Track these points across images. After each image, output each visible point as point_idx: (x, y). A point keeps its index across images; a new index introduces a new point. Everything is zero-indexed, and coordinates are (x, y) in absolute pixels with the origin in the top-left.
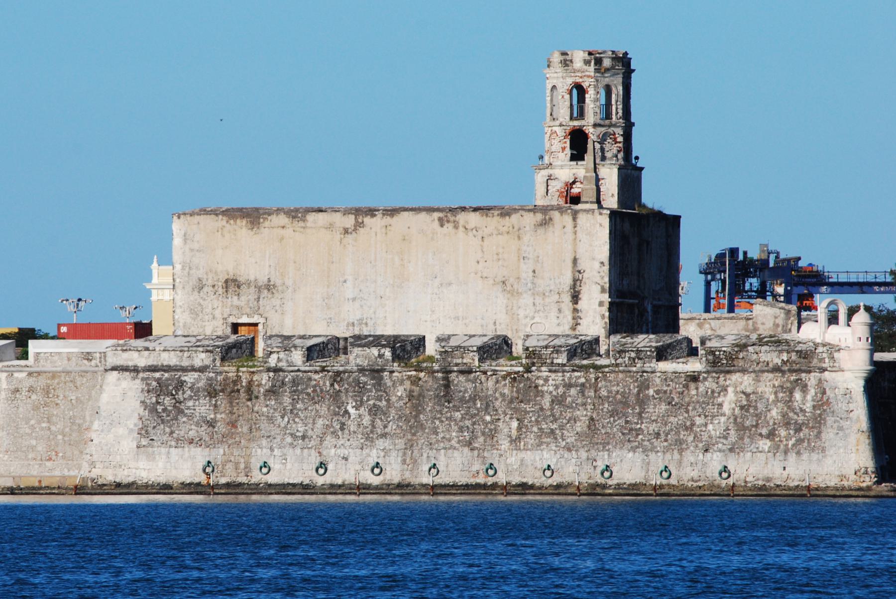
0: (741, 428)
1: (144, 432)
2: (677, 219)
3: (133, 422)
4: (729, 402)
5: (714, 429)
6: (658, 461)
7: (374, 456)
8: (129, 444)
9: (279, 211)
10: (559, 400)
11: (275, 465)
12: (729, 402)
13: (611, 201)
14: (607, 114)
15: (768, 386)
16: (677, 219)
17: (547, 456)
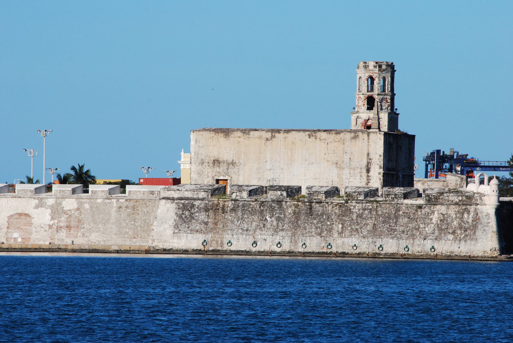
0: (440, 229)
1: (176, 226)
2: (413, 137)
3: (172, 222)
4: (435, 218)
5: (428, 230)
6: (403, 243)
7: (278, 239)
8: (170, 232)
9: (238, 130)
10: (360, 216)
11: (234, 242)
12: (435, 218)
13: (385, 128)
14: (383, 91)
15: (452, 211)
16: (413, 137)
17: (354, 240)
